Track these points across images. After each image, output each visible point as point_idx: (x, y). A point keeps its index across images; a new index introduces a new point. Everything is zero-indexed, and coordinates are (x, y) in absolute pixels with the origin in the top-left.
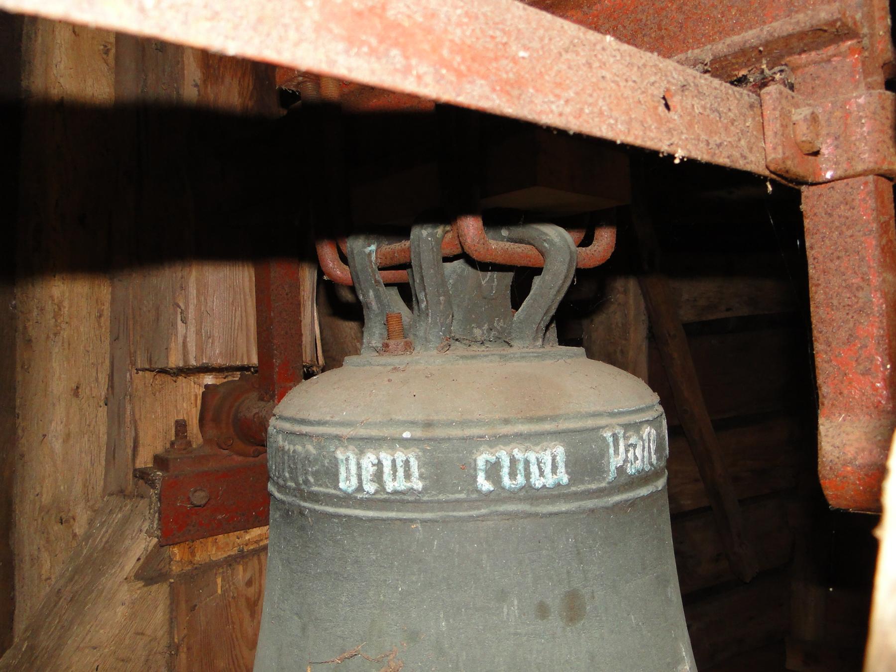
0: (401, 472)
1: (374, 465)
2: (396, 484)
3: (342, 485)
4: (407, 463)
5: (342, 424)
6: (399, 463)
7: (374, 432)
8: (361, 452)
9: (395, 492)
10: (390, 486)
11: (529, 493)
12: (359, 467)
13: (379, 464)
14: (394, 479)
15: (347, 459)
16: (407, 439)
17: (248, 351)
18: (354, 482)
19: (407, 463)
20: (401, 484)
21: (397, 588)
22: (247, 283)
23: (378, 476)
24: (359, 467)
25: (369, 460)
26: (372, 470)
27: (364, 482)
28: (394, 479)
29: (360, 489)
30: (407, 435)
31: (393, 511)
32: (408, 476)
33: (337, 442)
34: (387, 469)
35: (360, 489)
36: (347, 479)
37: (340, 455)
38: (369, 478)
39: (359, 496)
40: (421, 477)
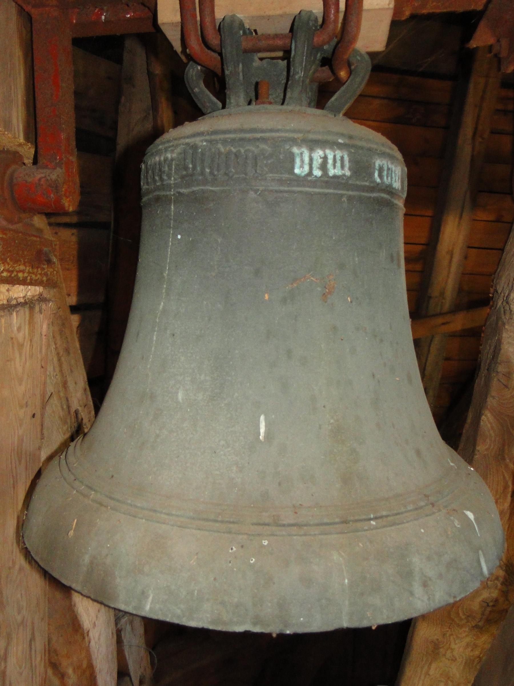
0: (338, 164)
1: (321, 158)
2: (336, 171)
3: (297, 171)
4: (342, 158)
5: (271, 131)
6: (338, 157)
7: (320, 137)
8: (311, 150)
9: (335, 177)
10: (332, 172)
11: (328, 181)
12: (311, 159)
13: (325, 159)
14: (335, 167)
15: (302, 154)
16: (340, 144)
17: (18, 125)
18: (306, 168)
19: (342, 158)
20: (338, 171)
21: (332, 237)
22: (20, 97)
23: (323, 167)
24: (311, 159)
25: (318, 154)
26: (320, 161)
27: (314, 169)
28: (335, 167)
29: (310, 173)
30: (340, 141)
31: (331, 189)
32: (343, 167)
33: (291, 143)
34: (330, 161)
35: (310, 173)
36: (302, 166)
37: (295, 150)
38: (318, 166)
39: (309, 178)
40: (350, 169)
